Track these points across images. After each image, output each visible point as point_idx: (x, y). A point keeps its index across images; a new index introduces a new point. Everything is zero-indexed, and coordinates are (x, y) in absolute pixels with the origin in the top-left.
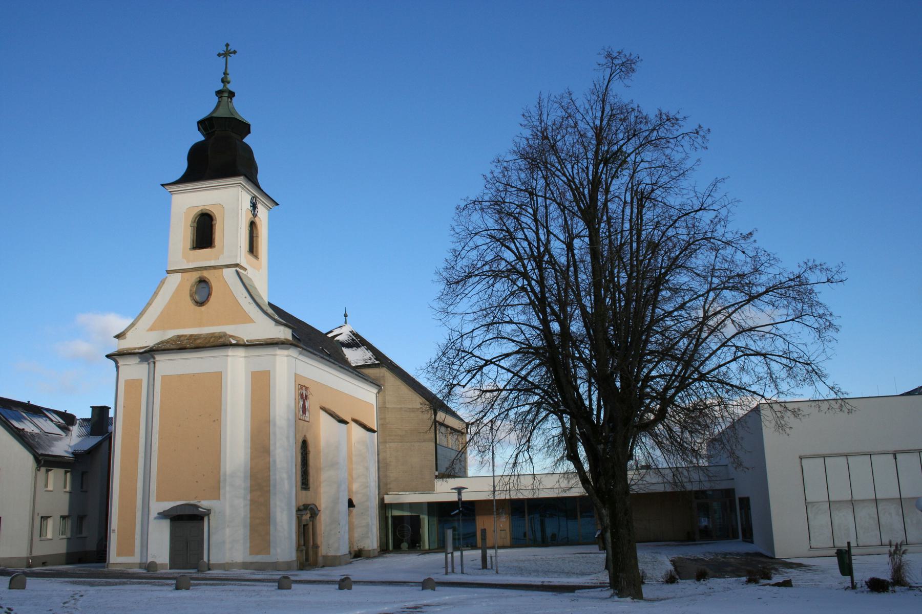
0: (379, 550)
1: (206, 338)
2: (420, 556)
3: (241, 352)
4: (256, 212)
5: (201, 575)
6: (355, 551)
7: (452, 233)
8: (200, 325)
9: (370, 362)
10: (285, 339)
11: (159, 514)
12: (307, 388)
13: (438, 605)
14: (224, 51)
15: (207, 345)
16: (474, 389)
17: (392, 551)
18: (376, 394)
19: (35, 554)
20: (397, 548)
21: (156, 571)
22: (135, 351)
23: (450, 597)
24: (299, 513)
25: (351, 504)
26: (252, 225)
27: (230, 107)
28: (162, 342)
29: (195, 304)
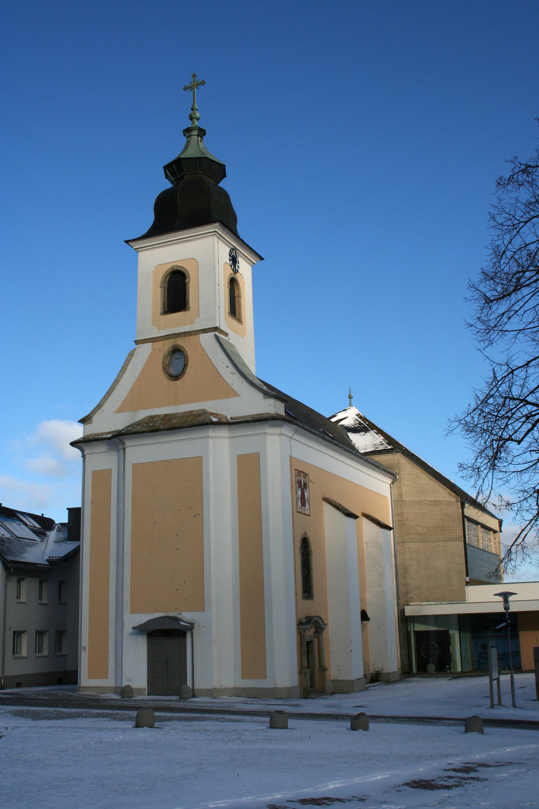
0: (400, 672)
1: (183, 417)
2: (451, 681)
3: (223, 433)
4: (237, 267)
5: (182, 704)
6: (372, 674)
7: (493, 223)
8: (176, 403)
9: (381, 448)
11: (133, 628)
12: (305, 475)
13: (500, 765)
14: (191, 83)
15: (184, 425)
16: (531, 451)
17: (416, 674)
18: (390, 485)
19: (8, 673)
20: (422, 671)
21: (132, 697)
22: (102, 436)
24: (302, 627)
25: (364, 616)
26: (233, 282)
27: (200, 146)
28: (132, 425)
29: (169, 377)
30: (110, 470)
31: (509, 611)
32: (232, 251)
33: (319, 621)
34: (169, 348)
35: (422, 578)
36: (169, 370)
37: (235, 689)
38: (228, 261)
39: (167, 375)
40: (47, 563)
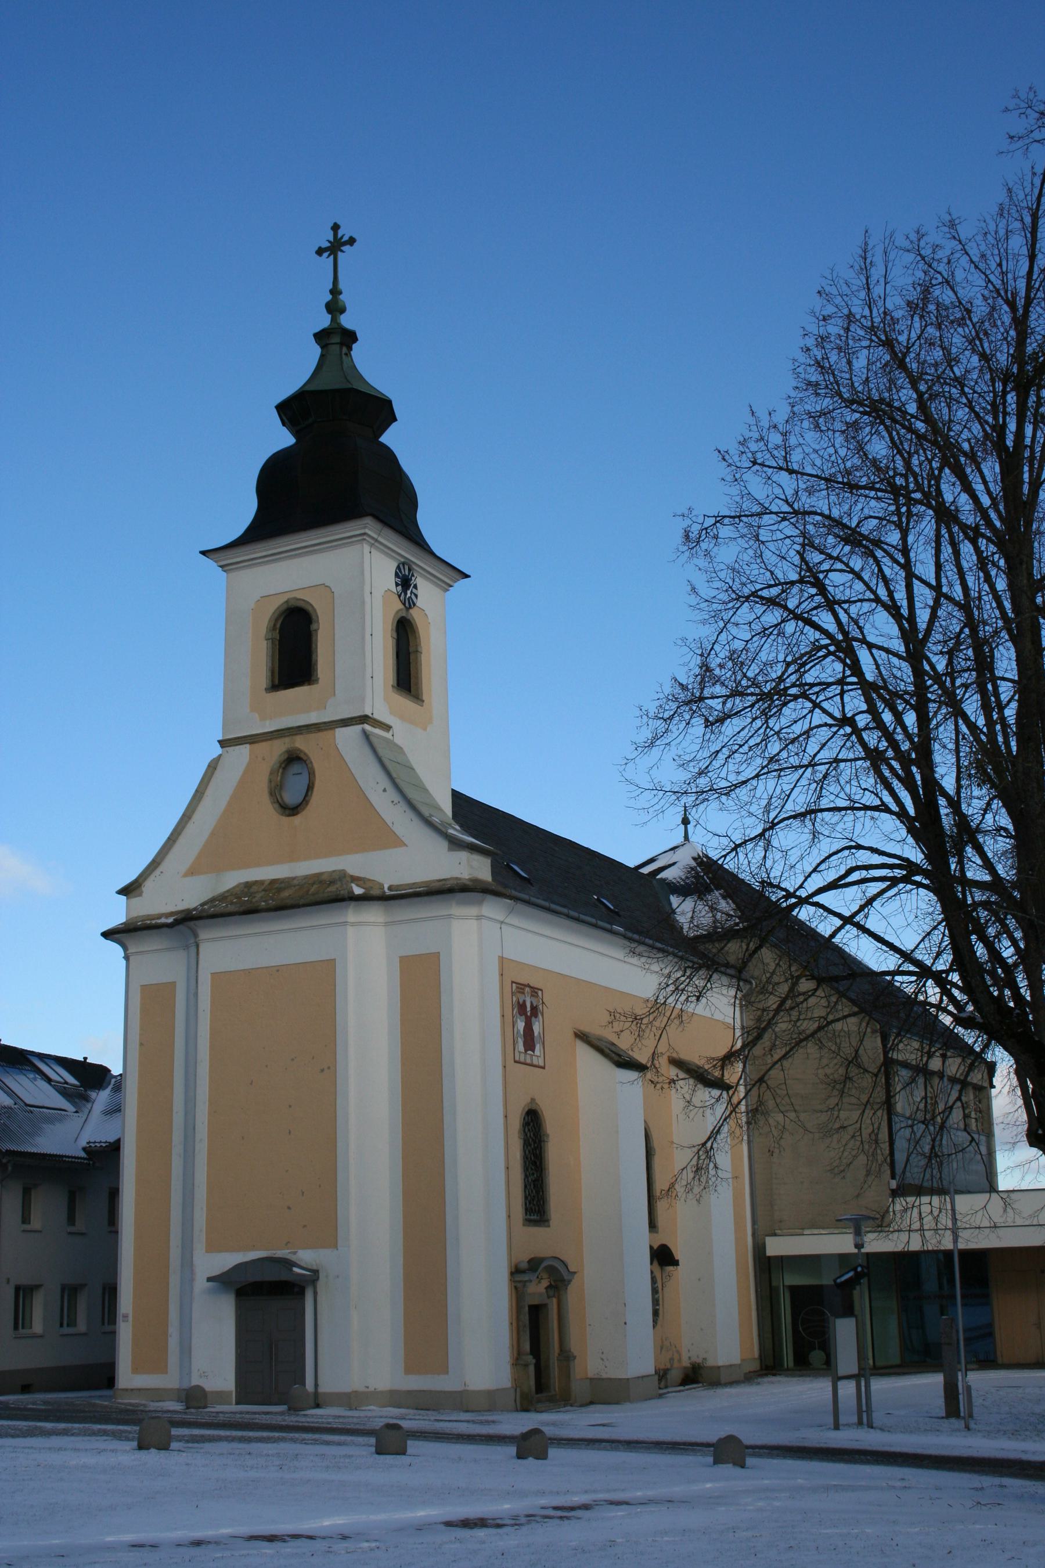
3: (373, 915)
5: (291, 1420)
6: (685, 1368)
7: (693, 600)
8: (293, 857)
10: (470, 880)
11: (209, 1279)
12: (535, 991)
14: (329, 241)
15: (302, 902)
21: (205, 1407)
22: (159, 921)
23: (717, 1485)
28: (212, 900)
30: (173, 984)
31: (863, 1250)
32: (401, 566)
33: (557, 1265)
34: (281, 755)
35: (802, 1183)
36: (281, 797)
37: (392, 1393)
38: (393, 588)
39: (277, 806)
40: (83, 1154)
